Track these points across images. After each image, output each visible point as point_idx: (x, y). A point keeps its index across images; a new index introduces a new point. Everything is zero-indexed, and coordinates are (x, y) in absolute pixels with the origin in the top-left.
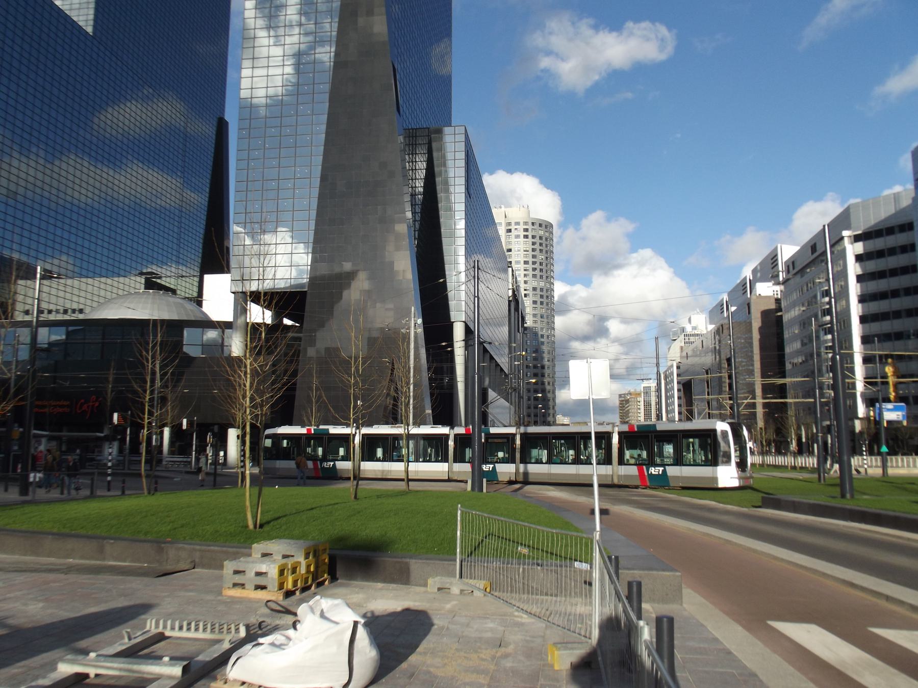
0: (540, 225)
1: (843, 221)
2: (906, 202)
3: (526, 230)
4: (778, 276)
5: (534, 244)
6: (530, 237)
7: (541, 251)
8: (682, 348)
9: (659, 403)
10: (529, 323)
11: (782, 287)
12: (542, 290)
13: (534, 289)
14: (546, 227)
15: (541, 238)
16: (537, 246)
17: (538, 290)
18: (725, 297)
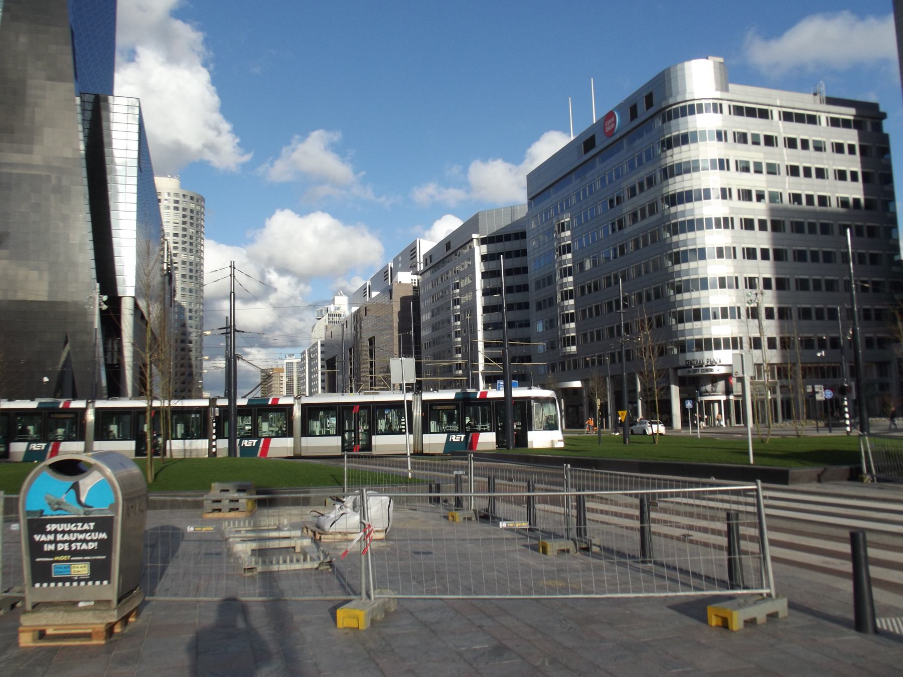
0: (192, 198)
1: (472, 225)
2: (521, 213)
3: (177, 202)
4: (416, 266)
5: (184, 216)
6: (181, 209)
7: (192, 224)
8: (326, 327)
9: (301, 379)
10: (178, 298)
11: (419, 277)
12: (191, 264)
13: (184, 263)
14: (198, 200)
15: (192, 211)
16: (187, 219)
17: (188, 264)
18: (369, 283)
